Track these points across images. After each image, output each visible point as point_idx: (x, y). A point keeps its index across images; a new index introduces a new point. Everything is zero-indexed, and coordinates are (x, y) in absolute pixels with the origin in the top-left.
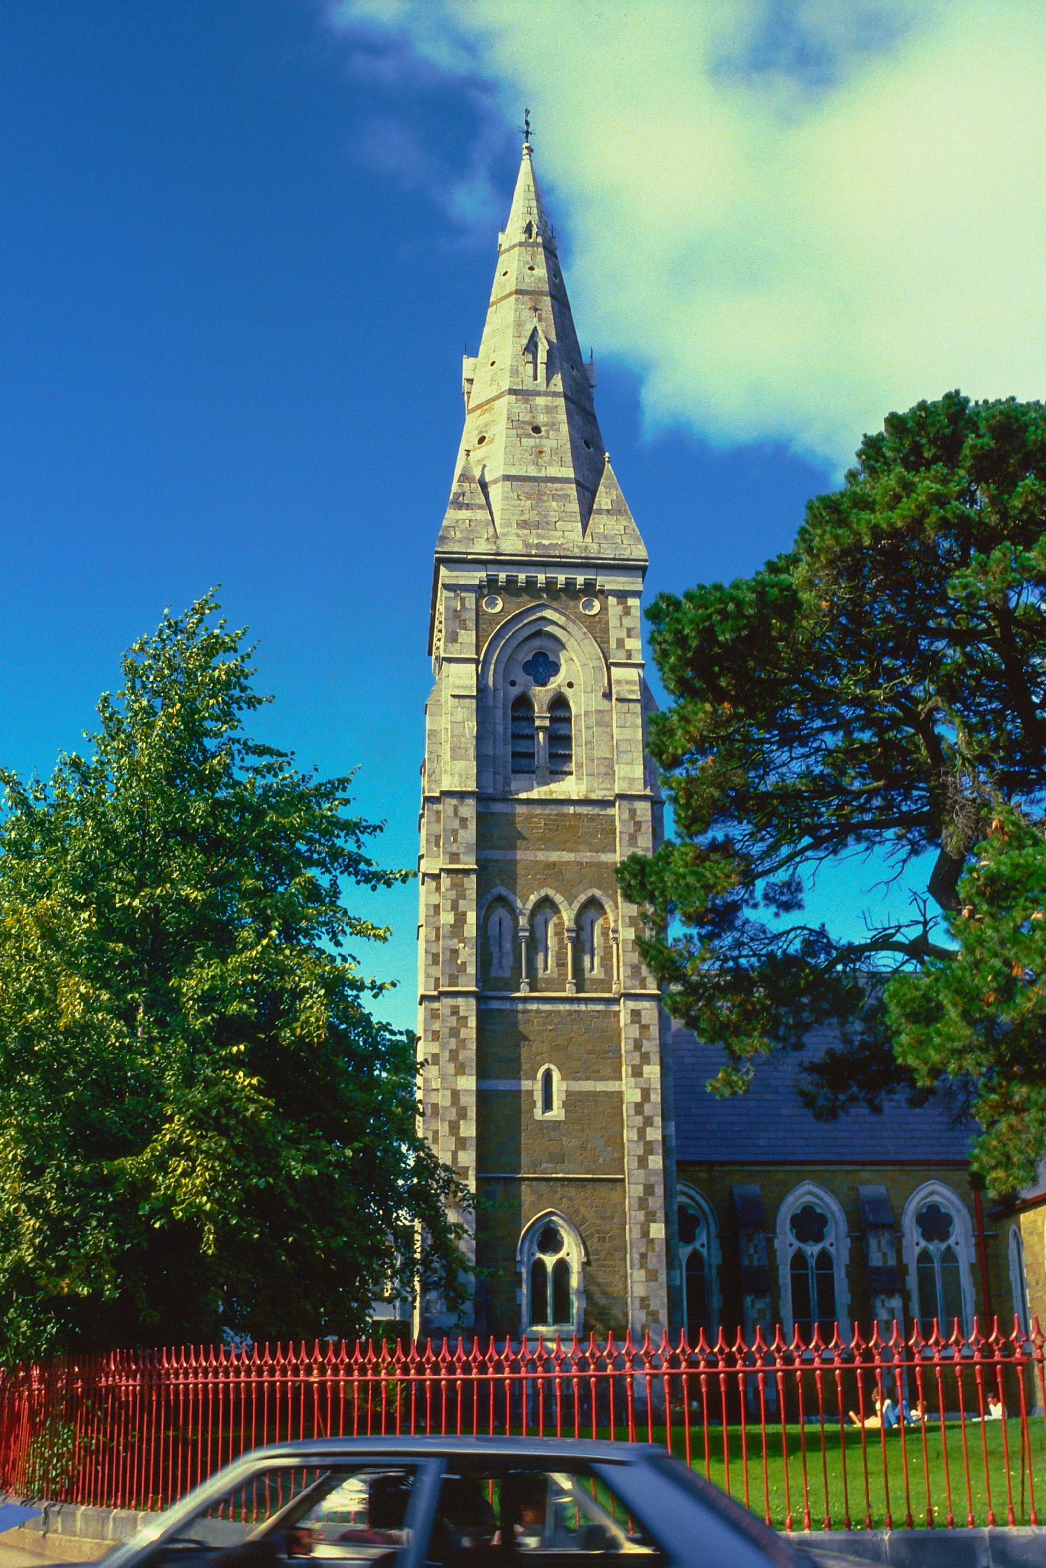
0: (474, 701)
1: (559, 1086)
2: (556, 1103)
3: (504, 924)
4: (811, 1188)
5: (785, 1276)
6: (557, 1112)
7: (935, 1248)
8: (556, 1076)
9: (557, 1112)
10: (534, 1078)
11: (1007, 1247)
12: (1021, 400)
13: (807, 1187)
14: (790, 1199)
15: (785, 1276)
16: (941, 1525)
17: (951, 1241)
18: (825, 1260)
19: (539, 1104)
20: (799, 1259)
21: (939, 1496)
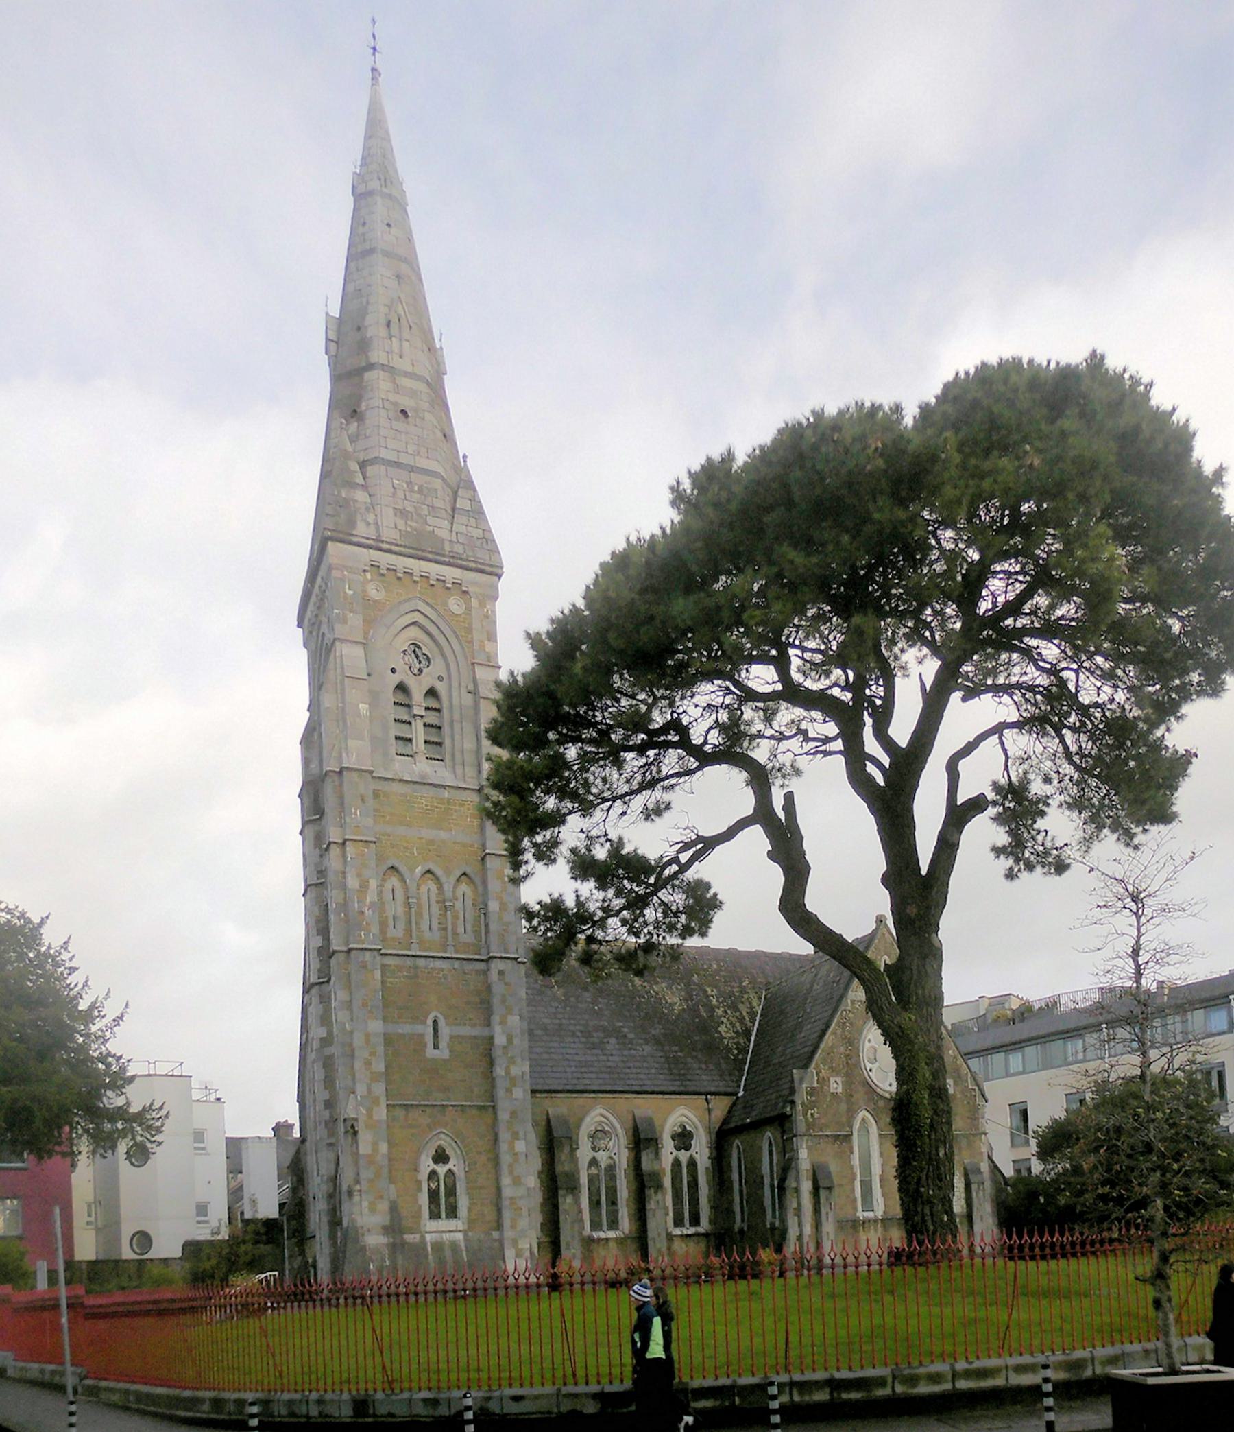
0: (841, 758)
1: (445, 1031)
2: (443, 1044)
3: (396, 892)
4: (686, 1112)
5: (584, 1180)
6: (444, 1053)
7: (684, 1156)
8: (442, 1023)
9: (444, 1053)
10: (424, 1023)
11: (730, 1156)
12: (831, 410)
13: (599, 1110)
14: (588, 1119)
15: (584, 1180)
16: (382, 1416)
17: (692, 1151)
18: (692, 1164)
19: (430, 1045)
20: (677, 1163)
21: (1093, 1271)
